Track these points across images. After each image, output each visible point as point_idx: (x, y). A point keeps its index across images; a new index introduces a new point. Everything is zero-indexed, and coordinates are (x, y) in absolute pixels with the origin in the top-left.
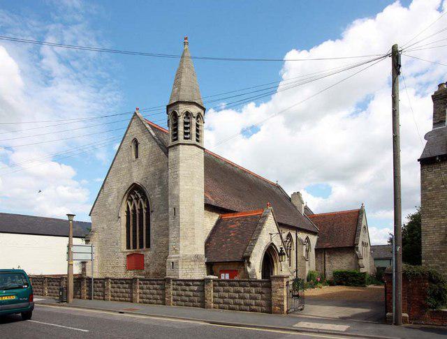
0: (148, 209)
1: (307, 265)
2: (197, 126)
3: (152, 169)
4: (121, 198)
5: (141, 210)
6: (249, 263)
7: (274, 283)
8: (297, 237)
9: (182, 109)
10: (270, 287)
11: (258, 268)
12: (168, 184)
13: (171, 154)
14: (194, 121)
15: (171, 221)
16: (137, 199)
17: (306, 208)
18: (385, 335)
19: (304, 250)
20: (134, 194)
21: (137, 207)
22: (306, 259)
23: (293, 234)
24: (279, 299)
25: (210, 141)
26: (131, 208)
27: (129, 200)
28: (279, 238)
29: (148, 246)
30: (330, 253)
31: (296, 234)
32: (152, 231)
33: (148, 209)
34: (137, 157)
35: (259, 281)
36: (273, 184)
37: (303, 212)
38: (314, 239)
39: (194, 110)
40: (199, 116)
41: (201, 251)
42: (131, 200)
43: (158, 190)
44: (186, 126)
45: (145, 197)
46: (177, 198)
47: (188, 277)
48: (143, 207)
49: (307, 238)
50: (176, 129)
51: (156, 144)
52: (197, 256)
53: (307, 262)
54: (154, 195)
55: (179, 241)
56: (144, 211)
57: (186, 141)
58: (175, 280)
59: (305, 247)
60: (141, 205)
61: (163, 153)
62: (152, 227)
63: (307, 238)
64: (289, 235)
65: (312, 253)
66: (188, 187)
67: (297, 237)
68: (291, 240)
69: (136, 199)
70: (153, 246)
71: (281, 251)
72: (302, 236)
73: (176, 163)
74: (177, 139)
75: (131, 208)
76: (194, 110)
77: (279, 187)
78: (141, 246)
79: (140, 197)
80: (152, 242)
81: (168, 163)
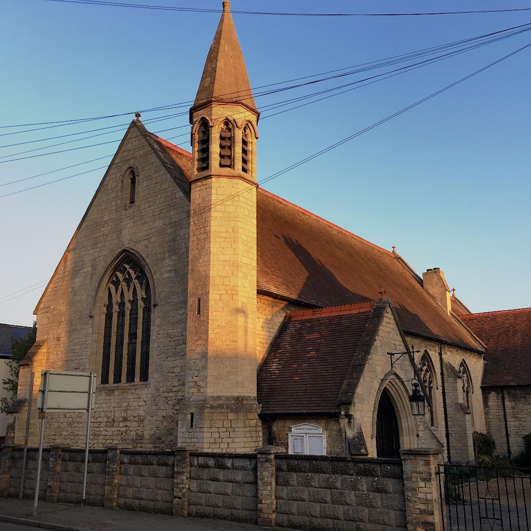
0: (147, 300)
1: (468, 425)
2: (245, 143)
3: (159, 224)
4: (96, 278)
5: (134, 303)
6: (349, 417)
7: (408, 467)
8: (441, 360)
9: (219, 113)
10: (399, 476)
11: (370, 429)
12: (187, 251)
13: (196, 192)
14: (239, 134)
15: (191, 324)
16: (128, 281)
17: (455, 300)
18: (43, 521)
19: (460, 390)
20: (124, 270)
21: (128, 296)
22: (465, 409)
23: (434, 355)
24: (422, 507)
25: (259, 169)
26: (116, 298)
27: (113, 282)
28: (408, 363)
29: (144, 377)
30: (514, 398)
31: (440, 354)
32: (154, 346)
33: (147, 300)
34: (132, 202)
35: (371, 461)
36: (386, 253)
37: (449, 308)
38: (476, 366)
39: (241, 115)
40: (248, 125)
41: (250, 390)
42: (117, 283)
43: (168, 263)
44: (224, 143)
45: (142, 276)
46: (205, 282)
47: (222, 449)
48: (139, 297)
49: (463, 364)
50: (205, 152)
51: (168, 176)
52: (239, 400)
53: (468, 417)
54: (161, 273)
55: (205, 367)
56: (128, 305)
57: (226, 171)
58: (195, 454)
59: (460, 383)
60: (135, 293)
61: (181, 194)
62: (153, 337)
63: (463, 364)
64: (426, 357)
65: (477, 395)
66: (227, 257)
67: (441, 360)
68: (431, 368)
69: (125, 280)
70: (154, 375)
71: (415, 392)
72: (453, 358)
73: (206, 209)
74: (207, 168)
75: (116, 298)
76: (241, 115)
77: (399, 259)
78: (118, 380)
79: (133, 276)
80: (151, 369)
81: (189, 211)
